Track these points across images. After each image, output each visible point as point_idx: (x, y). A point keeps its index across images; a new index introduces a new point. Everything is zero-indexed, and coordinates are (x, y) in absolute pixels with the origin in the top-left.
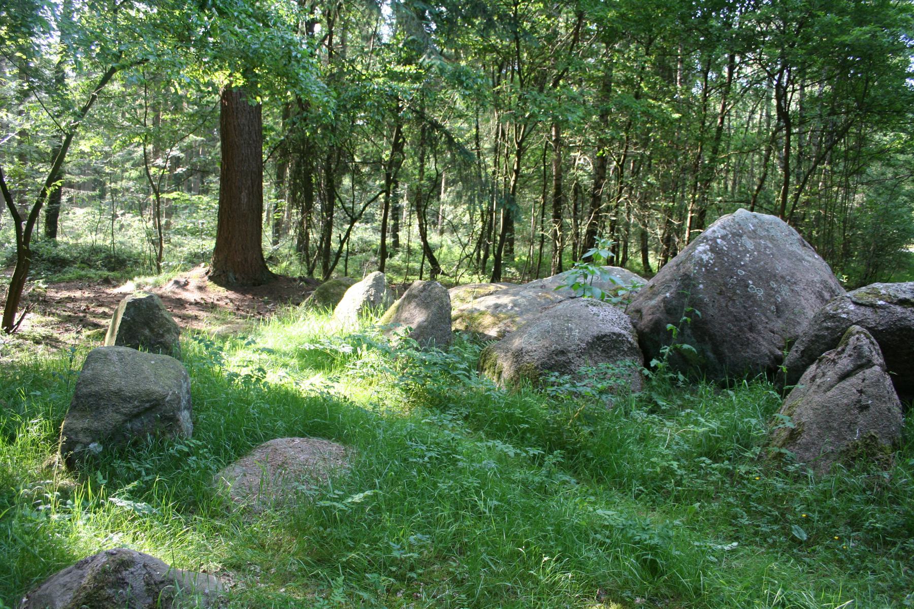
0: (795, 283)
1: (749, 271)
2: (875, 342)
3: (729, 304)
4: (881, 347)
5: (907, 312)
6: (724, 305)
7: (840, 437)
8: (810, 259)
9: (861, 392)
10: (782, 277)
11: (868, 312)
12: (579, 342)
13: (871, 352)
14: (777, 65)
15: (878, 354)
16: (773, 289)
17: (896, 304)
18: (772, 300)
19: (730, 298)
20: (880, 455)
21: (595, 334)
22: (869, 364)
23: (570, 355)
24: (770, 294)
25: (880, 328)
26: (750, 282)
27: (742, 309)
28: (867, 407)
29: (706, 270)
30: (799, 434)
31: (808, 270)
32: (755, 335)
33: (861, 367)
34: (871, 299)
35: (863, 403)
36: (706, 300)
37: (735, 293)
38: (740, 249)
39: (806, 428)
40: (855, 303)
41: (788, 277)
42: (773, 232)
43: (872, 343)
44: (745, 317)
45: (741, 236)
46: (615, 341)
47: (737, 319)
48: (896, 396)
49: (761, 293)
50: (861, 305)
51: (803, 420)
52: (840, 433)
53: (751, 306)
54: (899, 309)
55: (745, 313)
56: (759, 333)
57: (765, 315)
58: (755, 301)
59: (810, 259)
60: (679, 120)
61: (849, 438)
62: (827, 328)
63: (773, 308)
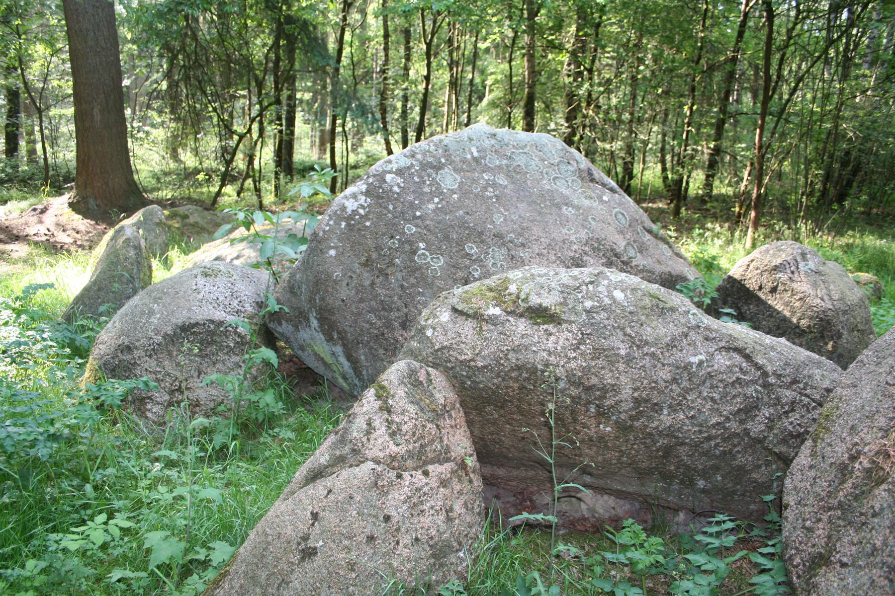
0: (523, 245)
3: (378, 281)
6: (367, 283)
8: (587, 203)
10: (499, 236)
12: (151, 334)
16: (468, 256)
19: (381, 271)
21: (180, 322)
23: (137, 353)
25: (480, 364)
26: (422, 245)
27: (398, 291)
29: (348, 225)
33: (339, 461)
36: (337, 274)
37: (391, 264)
38: (427, 189)
40: (455, 310)
42: (521, 160)
44: (399, 304)
45: (438, 168)
46: (212, 333)
47: (387, 308)
53: (413, 285)
54: (522, 326)
55: (400, 297)
58: (424, 278)
60: (851, 12)
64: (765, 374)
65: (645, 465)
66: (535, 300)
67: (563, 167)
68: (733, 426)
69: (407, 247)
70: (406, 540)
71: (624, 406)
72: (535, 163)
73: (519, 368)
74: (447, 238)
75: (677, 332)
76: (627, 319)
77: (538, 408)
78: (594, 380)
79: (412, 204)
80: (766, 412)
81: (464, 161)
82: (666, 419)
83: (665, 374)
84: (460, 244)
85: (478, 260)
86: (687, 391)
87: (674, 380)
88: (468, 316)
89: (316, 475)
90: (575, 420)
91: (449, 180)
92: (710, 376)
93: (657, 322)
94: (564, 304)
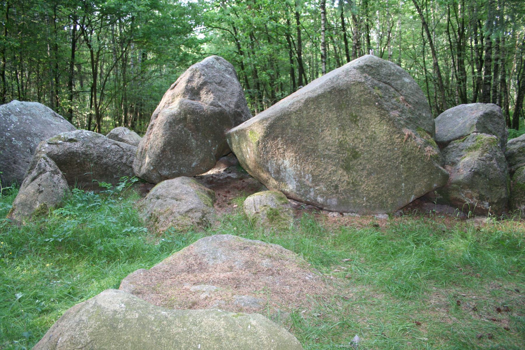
1: (13, 133)
5: (523, 143)
8: (57, 123)
9: (39, 185)
10: (35, 134)
13: (46, 166)
16: (28, 141)
18: (28, 146)
22: (45, 171)
24: (26, 144)
26: (13, 139)
27: (9, 153)
28: (42, 191)
32: (17, 165)
33: (40, 173)
35: (41, 190)
37: (5, 145)
38: (8, 122)
40: (49, 143)
42: (33, 111)
44: (11, 157)
45: (10, 115)
49: (20, 144)
50: (51, 144)
53: (14, 151)
54: (68, 144)
55: (11, 155)
56: (20, 164)
57: (23, 155)
58: (17, 149)
59: (57, 123)
63: (28, 150)
64: (123, 149)
65: (101, 173)
66: (69, 138)
67: (46, 112)
68: (119, 161)
69: (9, 140)
70: (60, 188)
71: (95, 158)
72: (38, 112)
73: (70, 153)
74: (20, 136)
75: (103, 141)
76: (91, 139)
77: (75, 163)
78: (88, 153)
79: (5, 127)
80: (125, 157)
81: (16, 112)
82: (105, 160)
83: (102, 150)
84: (25, 137)
85: (32, 142)
86: (108, 154)
87: (105, 151)
88: (53, 144)
89: (34, 179)
90: (84, 164)
91: (15, 119)
92: (112, 150)
93: (98, 139)
94: (76, 137)
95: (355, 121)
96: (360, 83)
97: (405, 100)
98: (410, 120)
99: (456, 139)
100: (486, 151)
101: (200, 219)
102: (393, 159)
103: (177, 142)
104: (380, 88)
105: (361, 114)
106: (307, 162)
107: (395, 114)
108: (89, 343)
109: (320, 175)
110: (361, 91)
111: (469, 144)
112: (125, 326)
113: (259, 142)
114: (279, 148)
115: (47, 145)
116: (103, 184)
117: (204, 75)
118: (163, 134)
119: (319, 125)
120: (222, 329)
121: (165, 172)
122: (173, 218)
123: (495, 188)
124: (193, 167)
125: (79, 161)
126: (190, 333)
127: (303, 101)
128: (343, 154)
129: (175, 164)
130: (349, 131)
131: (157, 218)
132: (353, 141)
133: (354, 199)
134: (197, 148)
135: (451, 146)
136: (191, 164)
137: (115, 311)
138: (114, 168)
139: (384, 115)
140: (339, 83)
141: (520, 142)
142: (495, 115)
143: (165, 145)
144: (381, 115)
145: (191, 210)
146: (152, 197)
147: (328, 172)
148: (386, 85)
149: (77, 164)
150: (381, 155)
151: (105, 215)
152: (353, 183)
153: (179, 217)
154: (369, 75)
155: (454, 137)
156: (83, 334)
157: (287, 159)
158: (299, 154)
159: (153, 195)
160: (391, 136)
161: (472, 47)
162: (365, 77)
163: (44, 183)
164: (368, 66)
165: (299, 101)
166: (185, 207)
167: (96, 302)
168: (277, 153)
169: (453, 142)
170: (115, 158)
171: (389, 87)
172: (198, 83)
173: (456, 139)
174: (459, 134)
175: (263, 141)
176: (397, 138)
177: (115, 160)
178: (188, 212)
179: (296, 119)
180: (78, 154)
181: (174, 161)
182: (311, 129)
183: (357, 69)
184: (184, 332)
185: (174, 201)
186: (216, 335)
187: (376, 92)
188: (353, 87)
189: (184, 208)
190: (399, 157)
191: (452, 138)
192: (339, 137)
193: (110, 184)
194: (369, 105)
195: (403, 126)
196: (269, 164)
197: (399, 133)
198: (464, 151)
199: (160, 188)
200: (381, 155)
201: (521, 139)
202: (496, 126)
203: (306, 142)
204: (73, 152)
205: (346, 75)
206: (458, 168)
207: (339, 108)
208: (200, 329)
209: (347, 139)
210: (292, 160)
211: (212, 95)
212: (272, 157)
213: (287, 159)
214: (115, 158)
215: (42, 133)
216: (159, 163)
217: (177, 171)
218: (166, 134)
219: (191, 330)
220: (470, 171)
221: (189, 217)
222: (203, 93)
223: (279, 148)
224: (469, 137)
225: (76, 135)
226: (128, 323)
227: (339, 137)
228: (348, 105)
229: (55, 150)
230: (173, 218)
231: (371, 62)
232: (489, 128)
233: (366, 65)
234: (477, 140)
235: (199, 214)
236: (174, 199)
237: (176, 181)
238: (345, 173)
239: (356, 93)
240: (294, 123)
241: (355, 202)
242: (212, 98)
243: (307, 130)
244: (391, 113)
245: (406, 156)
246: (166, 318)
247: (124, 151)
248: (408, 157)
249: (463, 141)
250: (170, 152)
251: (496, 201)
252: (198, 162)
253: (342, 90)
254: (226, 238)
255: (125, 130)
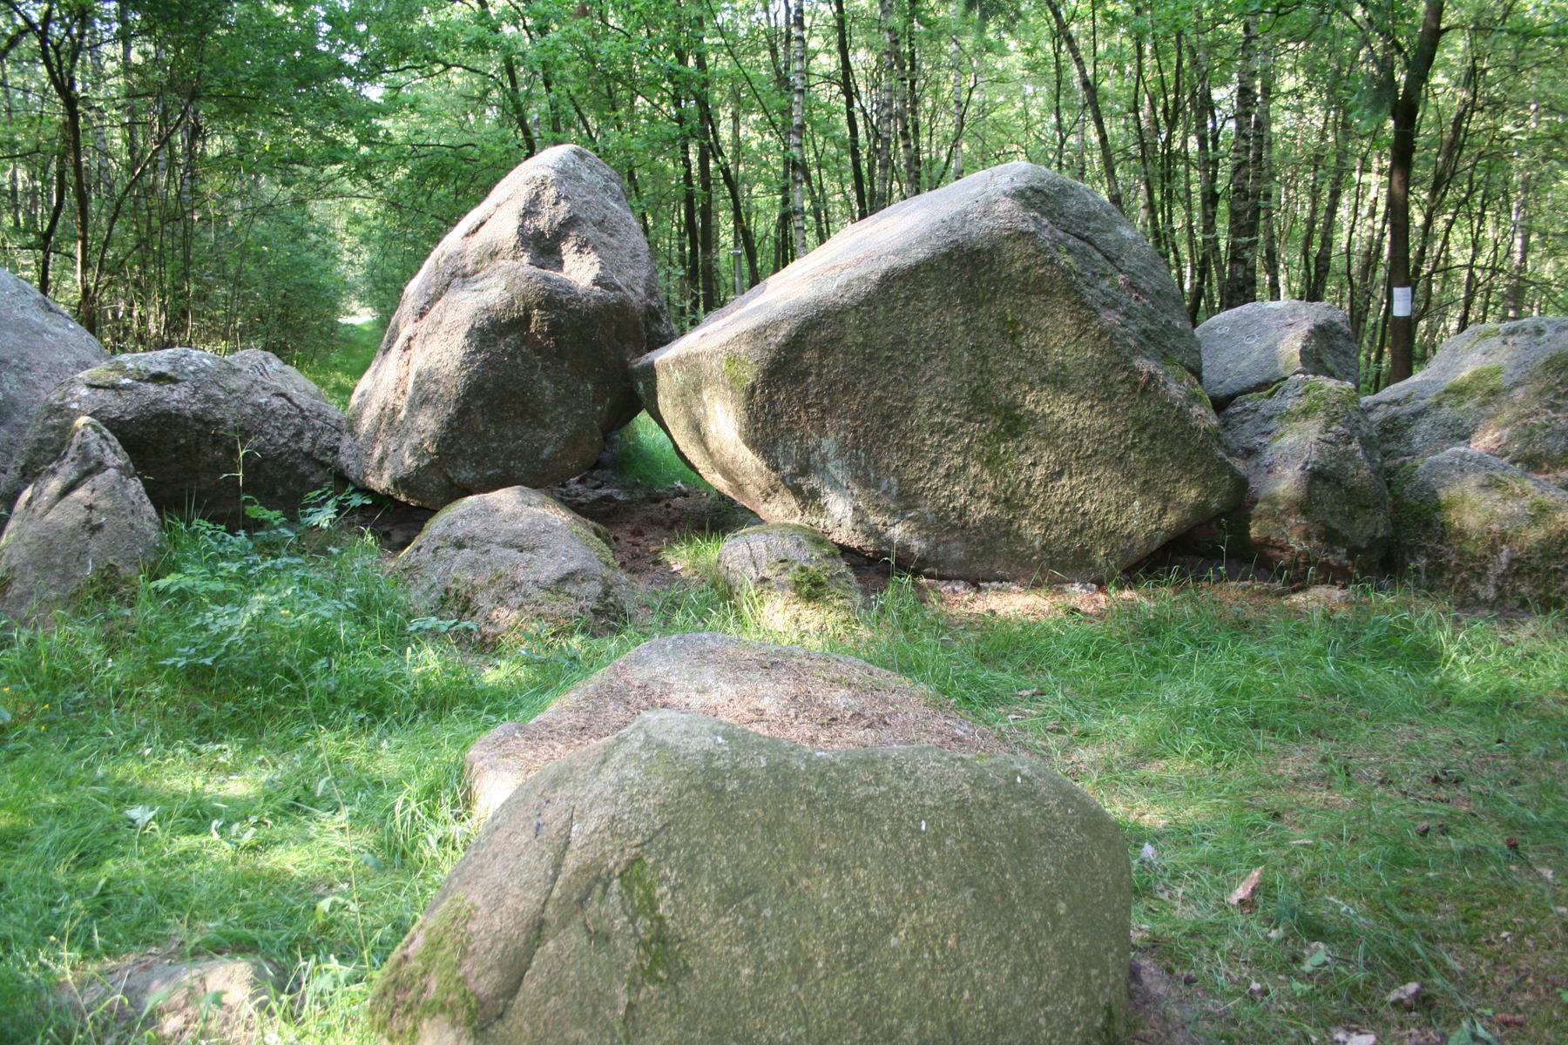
2: (110, 436)
4: (120, 441)
7: (66, 576)
8: (59, 330)
11: (108, 396)
13: (102, 450)
14: (1435, 869)
15: (115, 452)
17: (147, 381)
20: (123, 590)
22: (100, 467)
25: (128, 418)
28: (100, 527)
30: (9, 583)
31: (52, 348)
33: (89, 473)
34: (113, 377)
35: (95, 522)
39: (17, 573)
40: (90, 386)
41: (15, 361)
43: (104, 438)
48: (150, 509)
50: (98, 387)
51: (13, 563)
52: (66, 570)
54: (152, 388)
59: (59, 330)
61: (79, 574)
62: (54, 428)
64: (302, 411)
73: (157, 416)
78: (210, 417)
92: (273, 412)
94: (174, 370)
95: (1013, 337)
96: (1023, 233)
97: (1132, 286)
98: (1148, 338)
99: (1250, 390)
100: (1334, 420)
101: (599, 600)
102: (1112, 436)
103: (503, 386)
104: (1070, 251)
105: (1028, 318)
106: (885, 442)
107: (1110, 318)
108: (657, 833)
109: (920, 479)
110: (1029, 256)
111: (1291, 403)
112: (743, 784)
113: (753, 388)
114: (809, 406)
115: (84, 392)
116: (257, 511)
117: (566, 198)
118: (463, 363)
119: (918, 343)
120: (966, 786)
121: (465, 474)
122: (521, 599)
123: (1360, 512)
124: (543, 461)
125: (182, 441)
126: (897, 797)
127: (875, 277)
128: (981, 422)
129: (495, 450)
130: (996, 362)
131: (469, 600)
132: (1008, 388)
133: (1009, 543)
134: (555, 407)
135: (1238, 409)
136: (540, 450)
137: (709, 755)
138: (280, 466)
139: (1088, 320)
140: (970, 233)
141: (1383, 407)
142: (1339, 332)
143: (468, 394)
144: (1081, 321)
145: (569, 577)
146: (441, 543)
147: (942, 471)
148: (1083, 244)
149: (176, 450)
150: (1080, 425)
151: (262, 600)
152: (1007, 500)
153: (539, 595)
154: (1043, 214)
155: (1244, 385)
156: (639, 810)
157: (832, 435)
158: (864, 422)
159: (443, 537)
160: (1105, 377)
161: (1186, 157)
162: (1035, 219)
163: (104, 503)
164: (1037, 191)
165: (865, 279)
166: (551, 568)
167: (648, 736)
168: (804, 418)
169: (1243, 398)
170: (281, 435)
171: (1090, 248)
172: (551, 221)
173: (1250, 390)
174: (1257, 378)
175: (767, 383)
176: (1122, 382)
177: (282, 441)
178: (563, 580)
179: (858, 327)
180: (181, 420)
181: (493, 440)
182: (897, 354)
183: (1013, 196)
184: (882, 794)
185: (514, 553)
186: (955, 797)
187: (1066, 260)
188: (1009, 245)
189: (549, 570)
190: (1127, 432)
191: (1237, 389)
192: (972, 375)
193: (277, 513)
194: (1047, 293)
195: (1135, 352)
196: (780, 449)
197: (1125, 369)
198: (1275, 420)
199: (461, 515)
200: (1080, 425)
201: (1387, 399)
202: (1341, 359)
203: (884, 388)
204: (167, 414)
205: (985, 214)
206: (1267, 462)
207: (971, 300)
208: (915, 785)
209: (993, 382)
210: (846, 437)
211: (593, 257)
212: (790, 430)
213: (832, 435)
214: (281, 435)
215: (22, 360)
216: (450, 447)
217: (498, 471)
218: (472, 362)
219: (897, 789)
220: (1303, 468)
221: (569, 595)
222: (568, 250)
223: (809, 406)
224: (1285, 384)
225: (173, 362)
226: (749, 777)
227: (972, 375)
228: (994, 293)
229: (116, 405)
230: (521, 599)
231: (1042, 180)
232: (1329, 365)
233: (1032, 188)
234: (1307, 391)
235: (594, 588)
236: (512, 546)
237: (506, 499)
238: (986, 475)
239: (1017, 259)
240: (853, 338)
241: (1012, 552)
242: (597, 266)
243: (888, 358)
244: (1103, 316)
245: (1142, 429)
246: (833, 764)
247: (304, 418)
248: (1150, 431)
249: (1271, 395)
250: (483, 414)
251: (1364, 546)
252: (560, 445)
253: (978, 251)
254: (710, 642)
255: (266, 359)
